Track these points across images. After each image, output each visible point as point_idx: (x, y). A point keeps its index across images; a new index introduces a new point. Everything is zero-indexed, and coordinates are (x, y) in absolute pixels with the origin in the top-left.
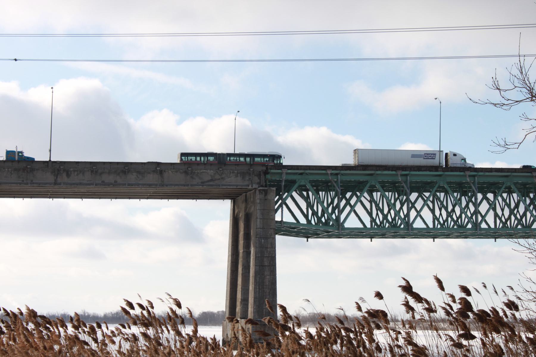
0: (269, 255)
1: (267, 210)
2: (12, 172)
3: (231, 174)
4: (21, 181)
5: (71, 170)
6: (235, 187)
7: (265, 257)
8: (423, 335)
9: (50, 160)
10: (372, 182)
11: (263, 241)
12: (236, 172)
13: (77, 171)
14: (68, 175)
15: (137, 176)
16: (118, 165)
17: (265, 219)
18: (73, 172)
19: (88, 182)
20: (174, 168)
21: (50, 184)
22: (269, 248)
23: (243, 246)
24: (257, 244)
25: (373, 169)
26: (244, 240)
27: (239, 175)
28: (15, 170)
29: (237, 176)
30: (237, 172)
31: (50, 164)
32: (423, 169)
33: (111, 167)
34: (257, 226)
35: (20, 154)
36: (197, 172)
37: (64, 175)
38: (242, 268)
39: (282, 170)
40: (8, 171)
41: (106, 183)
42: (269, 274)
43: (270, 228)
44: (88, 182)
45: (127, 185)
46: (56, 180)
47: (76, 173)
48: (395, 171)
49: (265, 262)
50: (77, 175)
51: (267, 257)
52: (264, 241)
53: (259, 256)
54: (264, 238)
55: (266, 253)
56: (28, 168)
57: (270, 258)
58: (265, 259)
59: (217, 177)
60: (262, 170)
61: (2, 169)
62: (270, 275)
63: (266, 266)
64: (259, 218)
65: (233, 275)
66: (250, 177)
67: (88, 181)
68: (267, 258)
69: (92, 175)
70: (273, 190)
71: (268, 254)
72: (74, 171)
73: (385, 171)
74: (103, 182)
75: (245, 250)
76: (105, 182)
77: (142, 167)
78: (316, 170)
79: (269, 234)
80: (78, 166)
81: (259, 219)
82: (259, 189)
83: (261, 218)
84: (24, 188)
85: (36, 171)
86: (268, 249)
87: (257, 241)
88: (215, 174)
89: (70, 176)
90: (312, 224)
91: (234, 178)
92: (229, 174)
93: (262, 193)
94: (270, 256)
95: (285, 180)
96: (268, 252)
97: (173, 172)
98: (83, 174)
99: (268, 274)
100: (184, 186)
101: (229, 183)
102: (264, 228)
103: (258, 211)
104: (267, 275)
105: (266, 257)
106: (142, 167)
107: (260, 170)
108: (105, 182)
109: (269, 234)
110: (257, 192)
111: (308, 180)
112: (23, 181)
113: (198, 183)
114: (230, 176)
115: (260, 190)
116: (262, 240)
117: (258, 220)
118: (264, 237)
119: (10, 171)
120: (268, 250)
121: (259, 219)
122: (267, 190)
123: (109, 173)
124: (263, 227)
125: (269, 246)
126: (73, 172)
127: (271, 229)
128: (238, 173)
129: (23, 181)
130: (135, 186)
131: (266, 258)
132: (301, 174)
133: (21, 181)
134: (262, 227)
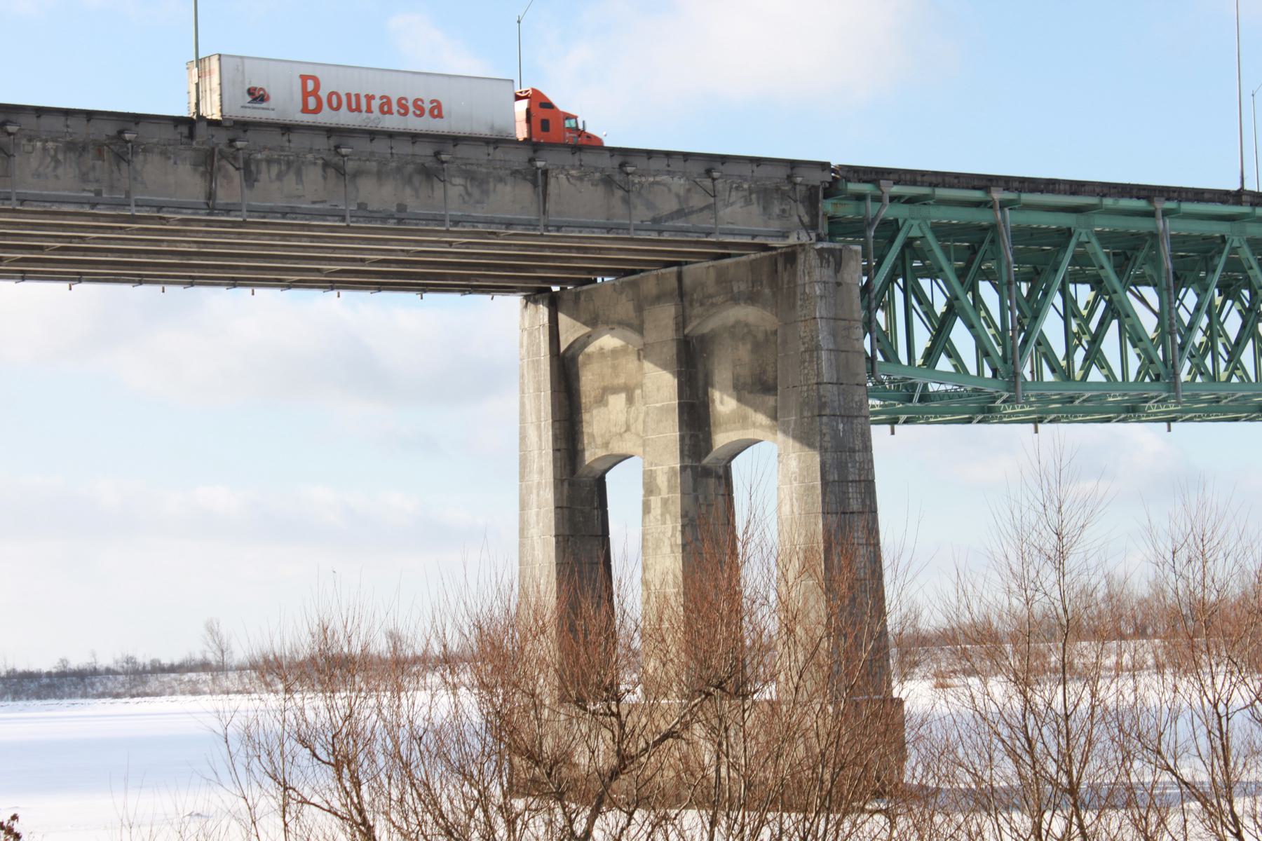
0: (860, 476)
1: (845, 320)
2: (60, 157)
3: (733, 193)
4: (92, 195)
5: (259, 156)
6: (748, 240)
7: (850, 484)
8: (222, 734)
9: (1242, 188)
10: (1233, 241)
11: (841, 426)
12: (746, 186)
13: (278, 161)
14: (250, 177)
15: (466, 188)
16: (685, 161)
17: (842, 351)
18: (264, 166)
19: (317, 206)
20: (581, 165)
21: (195, 208)
22: (859, 451)
23: (682, 452)
24: (827, 438)
25: (1094, 190)
26: (680, 429)
27: (754, 196)
28: (71, 147)
29: (748, 202)
30: (749, 187)
31: (201, 129)
32: (1067, 187)
33: (393, 151)
34: (819, 374)
35: (403, 102)
36: (639, 183)
37: (237, 177)
38: (683, 526)
39: (878, 187)
40: (45, 149)
41: (375, 212)
42: (864, 541)
43: (856, 382)
44: (317, 206)
45: (448, 223)
46: (211, 195)
47: (275, 170)
48: (930, 185)
49: (851, 500)
50: (280, 176)
51: (856, 481)
52: (843, 427)
53: (834, 481)
54: (842, 416)
55: (851, 470)
56: (127, 142)
57: (863, 484)
58: (850, 490)
59: (697, 200)
60: (822, 182)
61: (24, 142)
62: (866, 544)
63: (852, 513)
64: (826, 347)
65: (564, 552)
66: (783, 207)
67: (314, 203)
68: (854, 485)
69: (325, 178)
70: (856, 252)
71: (857, 471)
72: (269, 162)
73: (1123, 197)
74: (362, 206)
75: (688, 462)
76: (369, 208)
77: (489, 155)
78: (959, 187)
79: (856, 403)
80: (289, 141)
81: (827, 350)
82: (819, 246)
83: (831, 346)
84: (542, 247)
85: (141, 157)
86: (857, 454)
87: (823, 427)
88: (689, 190)
89: (256, 180)
90: (899, 362)
91: (741, 207)
92: (727, 193)
93: (828, 262)
94: (862, 478)
95: (881, 220)
96: (858, 464)
97: (571, 179)
98: (299, 173)
99: (860, 541)
100: (608, 233)
101: (728, 223)
102: (842, 384)
103: (821, 324)
104: (858, 544)
105: (852, 481)
106: (489, 155)
107: (817, 183)
108: (369, 208)
109: (856, 403)
110: (812, 254)
111: (929, 223)
112: (98, 193)
113: (642, 222)
114: (731, 201)
115: (820, 252)
116: (837, 424)
117: (824, 355)
118: (843, 413)
119: (52, 152)
120: (857, 458)
121: (827, 350)
122: (840, 250)
123: (380, 175)
124: (838, 379)
125: (858, 444)
126: (264, 166)
127: (857, 385)
128: (751, 191)
129: (98, 193)
130: (580, 232)
131: (852, 487)
132: (911, 200)
133: (92, 195)
134: (835, 381)
